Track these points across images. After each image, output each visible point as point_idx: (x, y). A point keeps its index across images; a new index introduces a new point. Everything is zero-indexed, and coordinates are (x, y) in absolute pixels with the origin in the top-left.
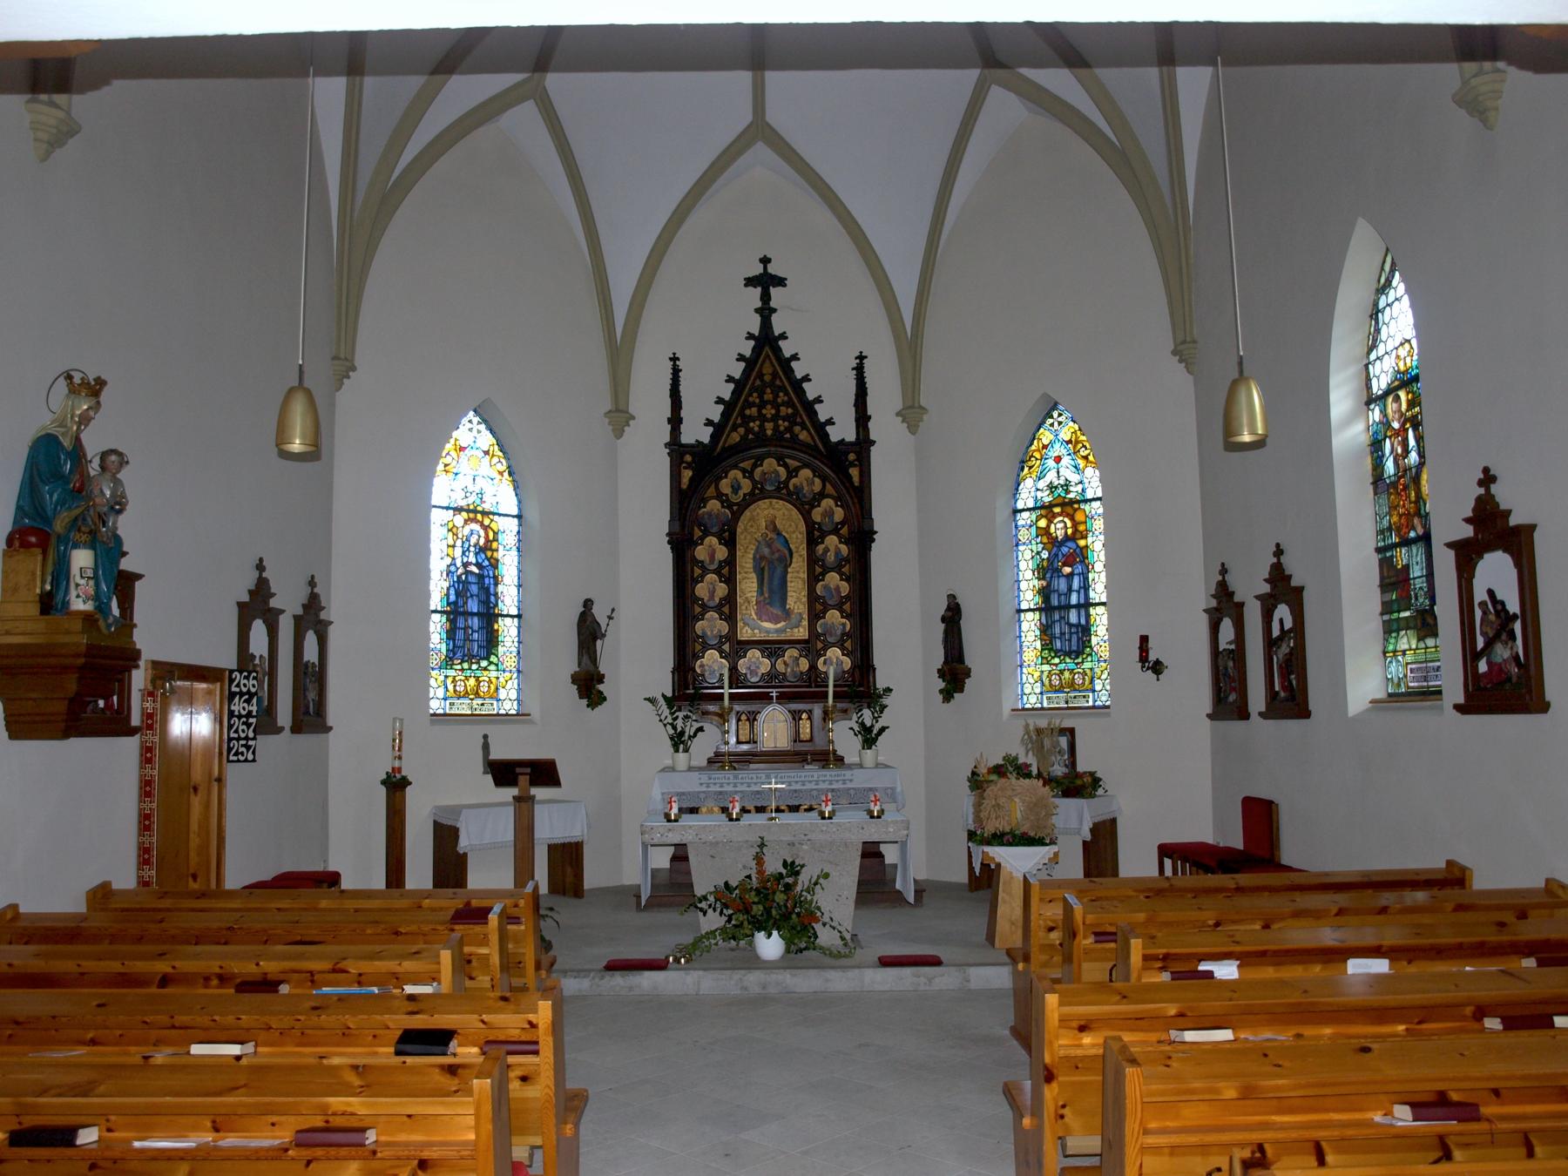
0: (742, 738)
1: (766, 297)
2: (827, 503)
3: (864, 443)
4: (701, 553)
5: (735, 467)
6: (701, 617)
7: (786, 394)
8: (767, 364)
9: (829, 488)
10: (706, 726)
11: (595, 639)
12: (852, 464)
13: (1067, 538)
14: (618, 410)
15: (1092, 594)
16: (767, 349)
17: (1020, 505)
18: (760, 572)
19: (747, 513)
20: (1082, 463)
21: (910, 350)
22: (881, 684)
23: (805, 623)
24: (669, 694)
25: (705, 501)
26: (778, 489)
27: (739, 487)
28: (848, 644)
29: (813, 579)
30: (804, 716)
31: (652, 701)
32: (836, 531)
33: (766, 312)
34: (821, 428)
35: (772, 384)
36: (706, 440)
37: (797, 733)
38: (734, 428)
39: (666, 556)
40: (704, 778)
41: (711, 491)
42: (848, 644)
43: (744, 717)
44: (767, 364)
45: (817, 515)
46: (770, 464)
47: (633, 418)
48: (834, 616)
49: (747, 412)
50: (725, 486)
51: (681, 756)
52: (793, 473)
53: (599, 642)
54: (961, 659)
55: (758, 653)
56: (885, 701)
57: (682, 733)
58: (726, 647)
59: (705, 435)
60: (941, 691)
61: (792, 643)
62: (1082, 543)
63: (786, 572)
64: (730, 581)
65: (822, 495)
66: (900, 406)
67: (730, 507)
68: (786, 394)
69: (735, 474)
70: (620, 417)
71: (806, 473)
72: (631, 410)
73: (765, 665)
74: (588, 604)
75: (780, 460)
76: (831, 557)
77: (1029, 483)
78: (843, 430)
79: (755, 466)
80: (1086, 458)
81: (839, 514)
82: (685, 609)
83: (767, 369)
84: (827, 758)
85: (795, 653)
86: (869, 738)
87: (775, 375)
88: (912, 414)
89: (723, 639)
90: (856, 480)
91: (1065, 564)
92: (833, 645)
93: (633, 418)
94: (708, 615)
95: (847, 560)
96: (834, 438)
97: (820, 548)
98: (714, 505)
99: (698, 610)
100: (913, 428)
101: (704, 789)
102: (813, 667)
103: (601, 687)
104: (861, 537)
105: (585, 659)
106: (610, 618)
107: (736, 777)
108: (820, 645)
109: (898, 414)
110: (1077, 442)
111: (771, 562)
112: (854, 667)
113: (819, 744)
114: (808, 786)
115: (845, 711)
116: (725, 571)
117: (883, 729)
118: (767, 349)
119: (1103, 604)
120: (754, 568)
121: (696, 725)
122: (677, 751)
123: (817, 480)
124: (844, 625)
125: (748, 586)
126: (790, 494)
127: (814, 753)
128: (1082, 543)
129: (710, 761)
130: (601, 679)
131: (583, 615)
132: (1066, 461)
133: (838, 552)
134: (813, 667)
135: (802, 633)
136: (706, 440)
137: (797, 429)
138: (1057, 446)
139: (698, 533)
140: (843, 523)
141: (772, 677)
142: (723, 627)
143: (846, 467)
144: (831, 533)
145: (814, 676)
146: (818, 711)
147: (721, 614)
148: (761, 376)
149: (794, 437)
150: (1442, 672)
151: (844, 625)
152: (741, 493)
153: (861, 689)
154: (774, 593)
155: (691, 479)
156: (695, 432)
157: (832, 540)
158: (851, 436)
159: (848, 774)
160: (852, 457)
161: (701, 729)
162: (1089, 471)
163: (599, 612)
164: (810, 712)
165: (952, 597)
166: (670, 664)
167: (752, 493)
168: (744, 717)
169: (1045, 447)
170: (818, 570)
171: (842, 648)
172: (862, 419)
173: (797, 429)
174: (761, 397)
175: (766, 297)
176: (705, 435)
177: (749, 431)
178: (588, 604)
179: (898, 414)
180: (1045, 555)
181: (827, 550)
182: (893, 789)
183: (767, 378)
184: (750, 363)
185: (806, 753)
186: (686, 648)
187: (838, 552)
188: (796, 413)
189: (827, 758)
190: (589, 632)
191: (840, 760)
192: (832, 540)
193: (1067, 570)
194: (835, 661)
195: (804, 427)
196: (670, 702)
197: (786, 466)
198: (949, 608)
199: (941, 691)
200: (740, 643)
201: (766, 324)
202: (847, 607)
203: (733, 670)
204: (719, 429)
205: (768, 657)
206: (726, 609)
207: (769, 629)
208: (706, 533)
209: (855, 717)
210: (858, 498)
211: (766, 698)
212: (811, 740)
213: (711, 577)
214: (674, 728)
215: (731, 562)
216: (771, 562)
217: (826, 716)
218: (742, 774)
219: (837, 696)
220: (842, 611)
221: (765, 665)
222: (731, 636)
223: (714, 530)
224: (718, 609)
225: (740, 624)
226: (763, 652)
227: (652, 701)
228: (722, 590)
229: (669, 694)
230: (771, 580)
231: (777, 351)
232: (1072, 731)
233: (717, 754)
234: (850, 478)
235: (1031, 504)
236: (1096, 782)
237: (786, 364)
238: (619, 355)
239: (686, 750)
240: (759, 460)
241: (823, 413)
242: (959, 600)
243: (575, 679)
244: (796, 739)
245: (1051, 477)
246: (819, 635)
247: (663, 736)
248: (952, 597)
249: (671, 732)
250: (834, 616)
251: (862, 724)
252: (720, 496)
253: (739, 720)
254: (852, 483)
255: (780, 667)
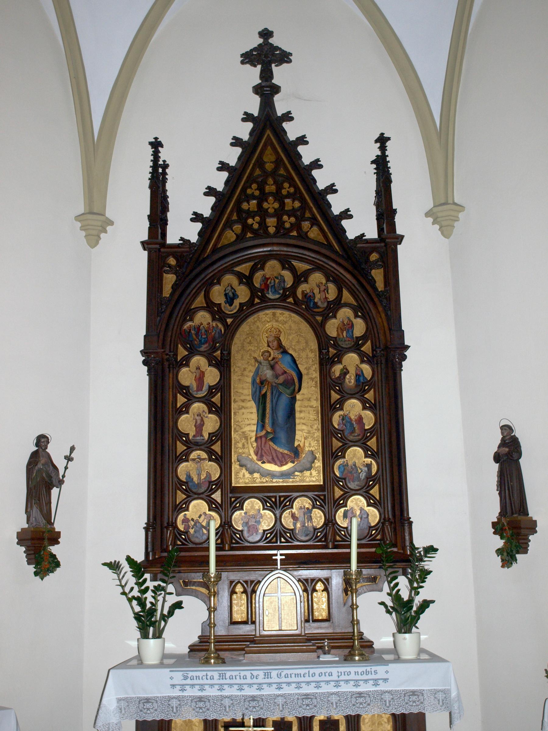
0: (237, 617)
1: (266, 75)
2: (345, 313)
3: (388, 239)
4: (186, 376)
5: (229, 270)
6: (185, 457)
7: (293, 184)
8: (269, 150)
9: (346, 295)
10: (187, 600)
11: (49, 487)
12: (375, 265)
14: (91, 213)
16: (268, 132)
18: (261, 401)
19: (245, 328)
21: (440, 141)
22: (420, 541)
23: (319, 464)
24: (140, 557)
25: (190, 313)
26: (284, 298)
27: (235, 296)
28: (375, 491)
29: (328, 408)
30: (320, 586)
31: (114, 566)
32: (356, 347)
33: (267, 90)
34: (334, 224)
35: (274, 173)
36: (194, 238)
37: (310, 609)
38: (229, 225)
39: (139, 379)
40: (178, 677)
41: (200, 301)
42: (375, 491)
43: (239, 588)
44: (269, 150)
45: (332, 328)
46: (272, 268)
47: (111, 223)
48: (356, 455)
49: (245, 206)
50: (217, 294)
51: (152, 644)
52: (300, 278)
53: (55, 491)
54: (523, 509)
55: (258, 504)
56: (427, 565)
57: (152, 612)
58: (217, 496)
59: (192, 232)
60: (499, 552)
61: (304, 490)
63: (293, 400)
64: (223, 411)
65: (335, 305)
66: (430, 205)
67: (222, 320)
68: (293, 184)
69: (229, 279)
70: (95, 222)
71: (317, 277)
72: (109, 214)
73: (267, 521)
74: (42, 441)
75: (285, 262)
76: (350, 380)
78: (362, 225)
79: (254, 270)
81: (359, 327)
82: (164, 444)
83: (269, 158)
84: (352, 646)
85: (306, 503)
86: (407, 615)
87: (278, 162)
88: (444, 213)
89: (213, 485)
90: (380, 285)
92: (356, 492)
93: (111, 223)
94: (194, 455)
95: (371, 384)
96: (351, 235)
97: (337, 369)
98: (203, 318)
99: (181, 448)
100: (446, 230)
101: (176, 693)
102: (330, 521)
103: (54, 549)
104: (388, 352)
105: (35, 511)
106: (69, 459)
107: (222, 676)
108: (338, 493)
109: (427, 215)
111: (273, 388)
112: (383, 520)
113: (340, 625)
114: (325, 689)
115: (373, 579)
116: (216, 399)
117: (425, 604)
118: (268, 132)
120: (254, 395)
121: (172, 600)
122: (145, 636)
123: (332, 287)
124: (369, 466)
125: (246, 418)
126: (297, 302)
127: (332, 638)
129: (193, 649)
130: (55, 538)
131: (34, 456)
133: (359, 375)
134: (330, 521)
135: (314, 477)
136: (194, 238)
137: (306, 225)
139: (182, 352)
140: (364, 338)
141: (278, 535)
142: (214, 470)
143: (368, 272)
144: (355, 443)
145: (331, 535)
146: (336, 578)
147: (210, 453)
148: (260, 163)
149: (303, 236)
151: (369, 466)
152: (237, 303)
153: (393, 550)
154: (278, 430)
155: (175, 287)
156: (182, 229)
157: (351, 359)
158: (372, 233)
159: (381, 670)
160: (374, 257)
161: (178, 605)
163: (56, 452)
164: (327, 581)
165: (507, 429)
166: (143, 519)
167: (251, 303)
168: (239, 588)
170: (335, 396)
171: (368, 497)
172: (385, 212)
173: (306, 225)
174: (261, 188)
175: (266, 75)
176: (192, 232)
177: (246, 228)
178: (42, 441)
179: (427, 215)
181: (345, 372)
182: (446, 692)
183: (269, 167)
184: (249, 148)
185: (320, 638)
186: (164, 492)
187: (359, 375)
188: (304, 206)
189: (352, 646)
190: (42, 477)
191: (369, 645)
192: (351, 359)
194: (359, 513)
195: (314, 222)
196: (138, 569)
197: (293, 270)
198: (503, 443)
199: (499, 552)
200: (235, 490)
201: (267, 104)
202: (372, 443)
203: (226, 525)
204: (209, 225)
205: (271, 509)
206: (217, 447)
207: (274, 472)
208: (193, 351)
209: (386, 588)
210: (381, 304)
211: (268, 563)
212: (328, 620)
213: (197, 407)
214: (141, 602)
215: (224, 387)
216: (273, 388)
217: (349, 586)
218: (230, 671)
219: (361, 558)
220: (366, 449)
221: (267, 521)
222: (223, 481)
223: (204, 348)
224: (207, 446)
225: (235, 467)
226: (264, 502)
227: (114, 566)
228: (212, 423)
229: (140, 557)
230: (274, 411)
231: (281, 134)
233: (204, 639)
234: (372, 283)
236: (54, 564)
237: (290, 149)
238: (96, 153)
239: (158, 635)
240: (260, 263)
241: (337, 204)
242: (517, 433)
243: (23, 538)
244: (309, 617)
246: (336, 480)
247: (126, 615)
248: (507, 429)
249: (138, 609)
250: (356, 455)
251: (397, 598)
252: (210, 307)
253: (233, 592)
254: (375, 289)
255: (287, 521)
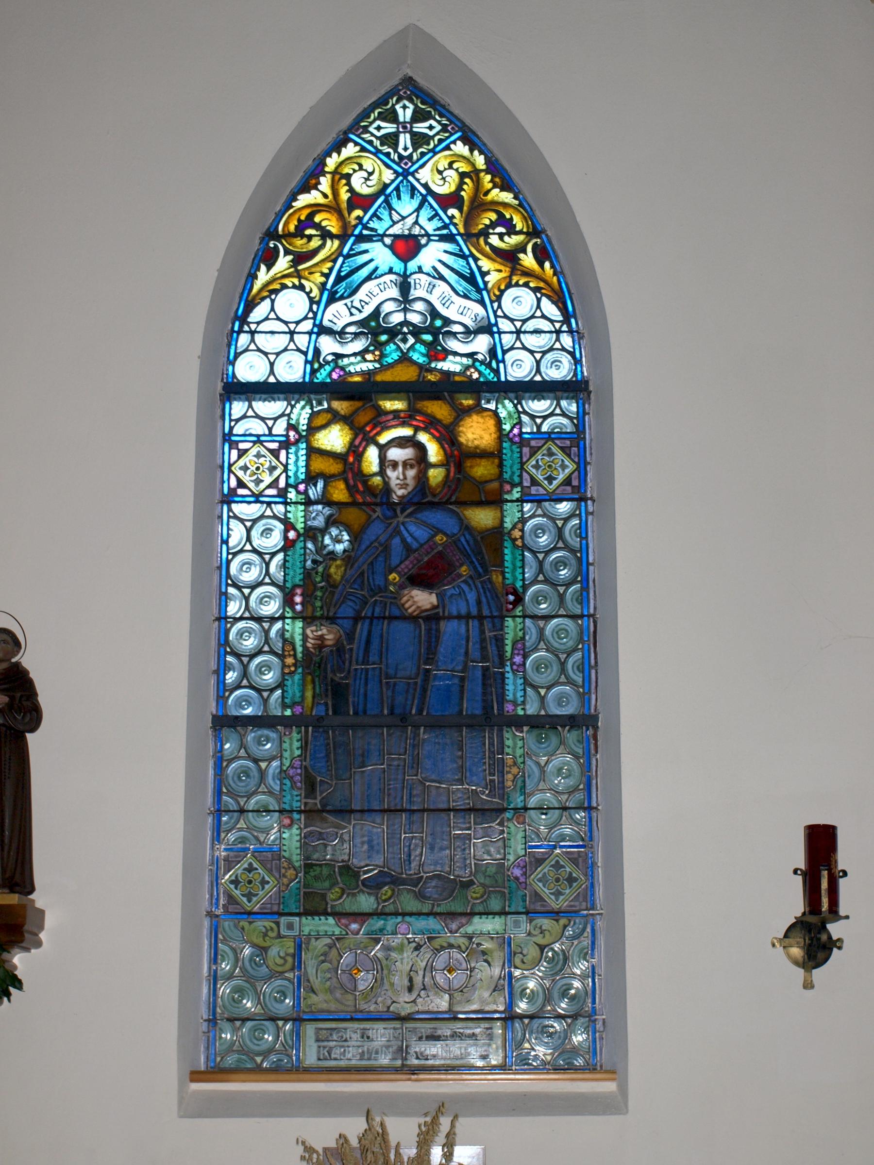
13: (422, 497)
15: (513, 686)
17: (249, 369)
20: (495, 273)
62: (482, 518)
77: (292, 304)
80: (509, 257)
91: (420, 580)
110: (479, 205)
119: (518, 722)
128: (482, 518)
132: (432, 254)
138: (406, 205)
150: (774, 949)
162: (519, 302)
169: (358, 201)
180: (338, 542)
193: (422, 599)
232: (319, 1059)
235: (291, 370)
245: (379, 295)
